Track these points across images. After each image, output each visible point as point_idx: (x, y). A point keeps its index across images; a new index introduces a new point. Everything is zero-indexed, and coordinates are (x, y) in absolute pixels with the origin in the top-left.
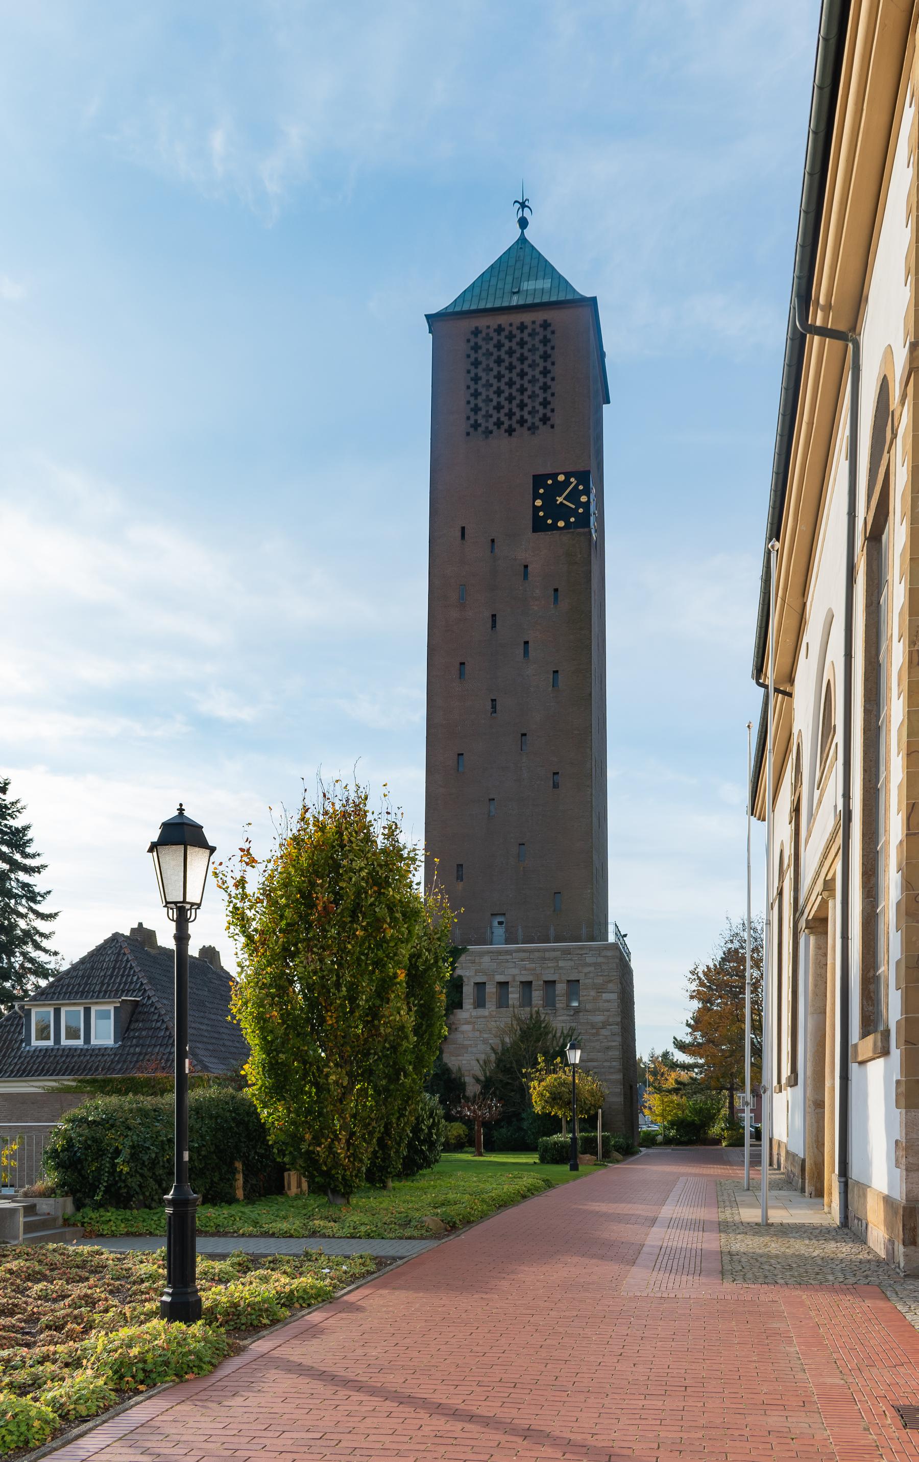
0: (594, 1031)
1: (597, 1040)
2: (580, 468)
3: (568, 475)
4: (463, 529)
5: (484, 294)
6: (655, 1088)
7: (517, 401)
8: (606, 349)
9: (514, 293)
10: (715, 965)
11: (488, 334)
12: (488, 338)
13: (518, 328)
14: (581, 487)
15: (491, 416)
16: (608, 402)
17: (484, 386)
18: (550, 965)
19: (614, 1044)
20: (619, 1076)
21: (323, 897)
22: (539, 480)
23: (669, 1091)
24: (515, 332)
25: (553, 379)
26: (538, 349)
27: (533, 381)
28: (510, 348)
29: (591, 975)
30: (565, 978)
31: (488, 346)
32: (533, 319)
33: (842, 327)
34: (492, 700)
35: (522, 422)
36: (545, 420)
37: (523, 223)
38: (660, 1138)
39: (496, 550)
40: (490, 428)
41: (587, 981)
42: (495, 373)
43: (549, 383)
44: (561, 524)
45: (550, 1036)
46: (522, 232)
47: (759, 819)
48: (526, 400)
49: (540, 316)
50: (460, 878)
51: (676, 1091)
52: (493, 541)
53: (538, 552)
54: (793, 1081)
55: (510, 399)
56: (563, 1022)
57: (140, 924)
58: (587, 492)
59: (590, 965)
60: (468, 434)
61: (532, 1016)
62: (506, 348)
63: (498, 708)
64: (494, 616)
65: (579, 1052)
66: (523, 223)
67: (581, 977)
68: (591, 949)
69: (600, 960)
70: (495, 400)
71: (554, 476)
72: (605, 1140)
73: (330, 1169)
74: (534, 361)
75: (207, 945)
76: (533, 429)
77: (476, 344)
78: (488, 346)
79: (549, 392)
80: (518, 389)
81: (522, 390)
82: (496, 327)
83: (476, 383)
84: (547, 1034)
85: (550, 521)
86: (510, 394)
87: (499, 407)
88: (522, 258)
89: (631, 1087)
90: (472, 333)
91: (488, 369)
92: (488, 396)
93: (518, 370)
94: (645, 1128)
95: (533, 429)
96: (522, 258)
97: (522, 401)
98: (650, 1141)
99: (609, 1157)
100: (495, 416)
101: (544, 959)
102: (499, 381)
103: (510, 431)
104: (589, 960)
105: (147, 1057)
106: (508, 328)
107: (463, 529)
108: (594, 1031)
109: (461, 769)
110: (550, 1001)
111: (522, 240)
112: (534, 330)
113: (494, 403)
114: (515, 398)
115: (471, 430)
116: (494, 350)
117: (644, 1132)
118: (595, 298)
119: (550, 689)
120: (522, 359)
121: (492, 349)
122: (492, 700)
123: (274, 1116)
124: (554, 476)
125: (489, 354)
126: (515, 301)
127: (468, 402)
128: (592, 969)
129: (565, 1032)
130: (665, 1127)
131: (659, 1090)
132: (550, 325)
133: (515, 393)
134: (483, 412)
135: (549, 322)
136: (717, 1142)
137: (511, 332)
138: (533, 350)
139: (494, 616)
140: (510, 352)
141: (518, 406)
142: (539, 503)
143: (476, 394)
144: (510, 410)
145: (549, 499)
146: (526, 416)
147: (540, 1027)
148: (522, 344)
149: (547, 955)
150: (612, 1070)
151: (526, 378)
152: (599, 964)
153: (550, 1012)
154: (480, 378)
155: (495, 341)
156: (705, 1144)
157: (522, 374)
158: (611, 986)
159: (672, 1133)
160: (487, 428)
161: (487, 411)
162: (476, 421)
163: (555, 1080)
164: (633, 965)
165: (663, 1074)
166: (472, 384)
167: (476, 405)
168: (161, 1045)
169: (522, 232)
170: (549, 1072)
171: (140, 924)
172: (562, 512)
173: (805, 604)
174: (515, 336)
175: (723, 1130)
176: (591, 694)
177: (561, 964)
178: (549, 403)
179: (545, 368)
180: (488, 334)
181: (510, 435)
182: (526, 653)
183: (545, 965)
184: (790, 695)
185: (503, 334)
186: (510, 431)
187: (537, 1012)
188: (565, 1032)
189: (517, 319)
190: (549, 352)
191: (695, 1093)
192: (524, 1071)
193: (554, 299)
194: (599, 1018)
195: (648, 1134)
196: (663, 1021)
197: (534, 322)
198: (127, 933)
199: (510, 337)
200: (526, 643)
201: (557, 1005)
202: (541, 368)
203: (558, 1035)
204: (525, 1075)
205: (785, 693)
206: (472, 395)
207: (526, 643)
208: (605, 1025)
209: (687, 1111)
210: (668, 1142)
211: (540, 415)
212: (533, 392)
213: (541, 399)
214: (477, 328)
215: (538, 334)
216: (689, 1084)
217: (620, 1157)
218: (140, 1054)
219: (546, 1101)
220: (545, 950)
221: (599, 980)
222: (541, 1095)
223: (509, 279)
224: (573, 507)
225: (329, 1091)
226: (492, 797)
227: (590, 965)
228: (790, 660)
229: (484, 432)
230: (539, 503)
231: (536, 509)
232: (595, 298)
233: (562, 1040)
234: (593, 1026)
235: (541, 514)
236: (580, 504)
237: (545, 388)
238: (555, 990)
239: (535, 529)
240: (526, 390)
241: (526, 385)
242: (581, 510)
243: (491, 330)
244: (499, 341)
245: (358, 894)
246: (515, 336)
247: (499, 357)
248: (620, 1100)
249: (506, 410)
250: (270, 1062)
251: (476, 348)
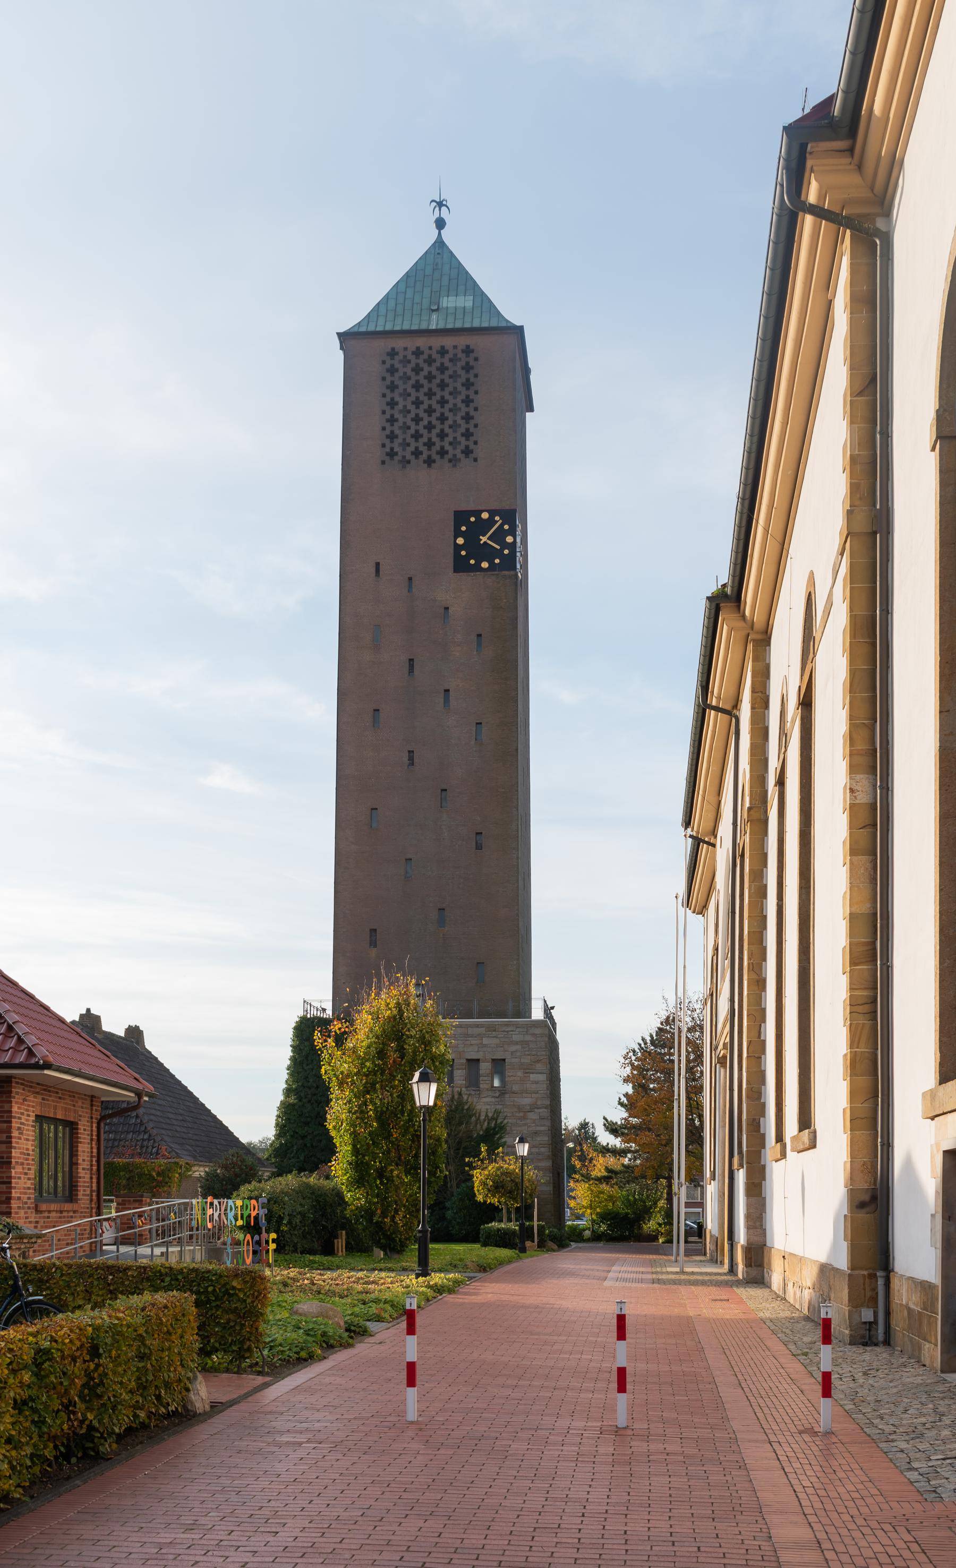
0: (521, 1114)
1: (525, 1124)
2: (506, 506)
3: (492, 513)
4: (378, 564)
5: (400, 308)
6: (582, 1175)
7: (437, 430)
8: (531, 364)
9: (433, 311)
10: (651, 1036)
11: (405, 357)
12: (406, 361)
14: (506, 527)
15: (408, 445)
16: (532, 410)
17: (400, 412)
18: (473, 1042)
19: (542, 1128)
20: (548, 1164)
21: (393, 1056)
22: (460, 517)
23: (600, 1180)
24: (435, 356)
25: (476, 409)
26: (460, 376)
27: (454, 410)
28: (430, 373)
29: (518, 1054)
30: (490, 1056)
31: (405, 370)
33: (728, 707)
34: (409, 752)
35: (442, 453)
36: (467, 452)
37: (440, 224)
38: (587, 1234)
39: (414, 590)
40: (407, 458)
41: (514, 1060)
42: (413, 398)
43: (472, 413)
44: (485, 565)
45: (473, 1118)
46: (440, 234)
47: (694, 912)
48: (447, 430)
49: (462, 341)
50: (373, 944)
51: (606, 1179)
52: (410, 579)
53: (461, 594)
54: (713, 1178)
55: (430, 427)
56: (487, 1103)
57: (88, 1010)
58: (513, 532)
59: (517, 1043)
60: (383, 462)
61: (453, 1097)
62: (425, 373)
63: (415, 760)
64: (411, 660)
65: (527, 1146)
66: (440, 224)
67: (507, 1056)
68: (517, 1026)
69: (528, 1038)
70: (413, 427)
71: (477, 513)
72: (541, 1229)
73: (392, 1234)
74: (455, 388)
75: (133, 1024)
76: (454, 461)
77: (392, 366)
78: (405, 370)
79: (472, 422)
80: (435, 409)
81: (443, 419)
82: (414, 349)
84: (470, 1117)
85: (472, 562)
86: (430, 423)
87: (417, 436)
89: (559, 1174)
90: (388, 354)
91: (406, 395)
92: (405, 423)
93: (438, 397)
94: (569, 1223)
95: (454, 461)
97: (442, 431)
98: (576, 1236)
99: (544, 1247)
100: (413, 445)
101: (467, 1035)
102: (417, 408)
103: (429, 462)
104: (516, 1038)
105: (122, 1143)
106: (427, 352)
107: (378, 564)
108: (521, 1114)
109: (374, 825)
110: (473, 1081)
111: (440, 244)
112: (455, 355)
113: (412, 431)
114: (434, 427)
115: (387, 459)
116: (412, 374)
117: (570, 1227)
119: (473, 742)
120: (443, 385)
121: (409, 373)
122: (409, 752)
123: (354, 1198)
124: (477, 513)
125: (406, 378)
126: (435, 322)
127: (384, 429)
128: (518, 1047)
129: (490, 1115)
130: (593, 1221)
131: (587, 1178)
132: (473, 351)
133: (434, 422)
134: (400, 440)
135: (471, 347)
136: (654, 1238)
137: (430, 356)
138: (454, 376)
139: (411, 660)
140: (430, 378)
141: (438, 435)
142: (460, 541)
143: (392, 420)
144: (430, 439)
145: (472, 537)
146: (447, 447)
147: (463, 1109)
148: (442, 369)
149: (470, 1031)
150: (540, 1157)
151: (447, 406)
152: (527, 1043)
153: (473, 1093)
154: (397, 404)
155: (413, 365)
156: (639, 1241)
157: (443, 402)
158: (539, 1066)
159: (603, 1228)
160: (404, 457)
161: (404, 439)
162: (392, 449)
163: (498, 1169)
164: (559, 1036)
165: (591, 1160)
166: (388, 409)
167: (392, 432)
168: (134, 1132)
169: (440, 234)
170: (491, 1162)
171: (88, 1010)
172: (485, 552)
173: (720, 802)
174: (435, 361)
175: (660, 1225)
176: (517, 750)
177: (485, 1041)
178: (472, 435)
179: (467, 396)
180: (405, 357)
181: (429, 466)
182: (447, 701)
183: (468, 1042)
184: (714, 845)
185: (422, 357)
186: (429, 462)
187: (460, 1094)
188: (490, 1115)
189: (437, 342)
190: (472, 380)
191: (628, 1182)
192: (467, 1160)
193: (476, 324)
194: (526, 1101)
195: (574, 1229)
196: (592, 1094)
197: (455, 347)
198: (122, 1033)
199: (430, 361)
200: (447, 691)
201: (481, 1086)
202: (463, 397)
203: (482, 1118)
204: (470, 1165)
205: (709, 843)
206: (387, 421)
207: (447, 691)
208: (533, 1107)
209: (619, 1204)
210: (597, 1237)
211: (462, 447)
212: (455, 421)
213: (463, 430)
214: (393, 349)
215: (460, 359)
216: (621, 1172)
217: (555, 1247)
218: (114, 1140)
219: (489, 1190)
220: (468, 1026)
221: (527, 1060)
222: (484, 1184)
223: (427, 292)
224: (498, 547)
225: (393, 1181)
226: (409, 856)
227: (517, 1043)
228: (712, 824)
229: (400, 462)
231: (458, 548)
232: (522, 327)
233: (486, 1124)
234: (520, 1108)
235: (463, 553)
236: (505, 545)
238: (478, 1069)
239: (456, 570)
240: (447, 419)
241: (447, 414)
242: (506, 552)
243: (409, 353)
244: (417, 365)
245: (414, 1052)
246: (435, 361)
247: (417, 381)
248: (550, 1188)
249: (425, 440)
250: (356, 1162)
251: (392, 370)
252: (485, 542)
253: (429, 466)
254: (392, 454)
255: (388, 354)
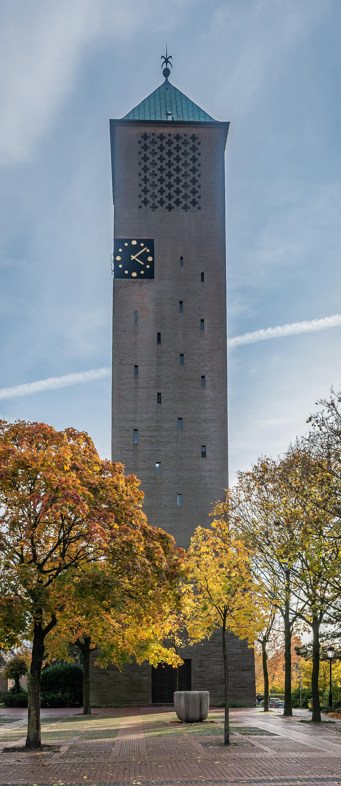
13: (175, 138)
17: (151, 174)
32: (153, 132)
36: (194, 203)
37: (166, 73)
43: (197, 178)
44: (134, 274)
46: (167, 79)
60: (140, 207)
66: (166, 73)
83: (145, 172)
85: (126, 272)
88: (167, 93)
96: (167, 93)
115: (143, 205)
118: (111, 121)
132: (197, 138)
143: (146, 180)
169: (167, 79)
181: (170, 210)
224: (143, 264)
229: (151, 207)
230: (118, 258)
235: (121, 266)
237: (194, 181)
242: (148, 267)
252: (134, 259)
253: (170, 210)
254: (146, 202)
255: (142, 137)
